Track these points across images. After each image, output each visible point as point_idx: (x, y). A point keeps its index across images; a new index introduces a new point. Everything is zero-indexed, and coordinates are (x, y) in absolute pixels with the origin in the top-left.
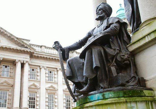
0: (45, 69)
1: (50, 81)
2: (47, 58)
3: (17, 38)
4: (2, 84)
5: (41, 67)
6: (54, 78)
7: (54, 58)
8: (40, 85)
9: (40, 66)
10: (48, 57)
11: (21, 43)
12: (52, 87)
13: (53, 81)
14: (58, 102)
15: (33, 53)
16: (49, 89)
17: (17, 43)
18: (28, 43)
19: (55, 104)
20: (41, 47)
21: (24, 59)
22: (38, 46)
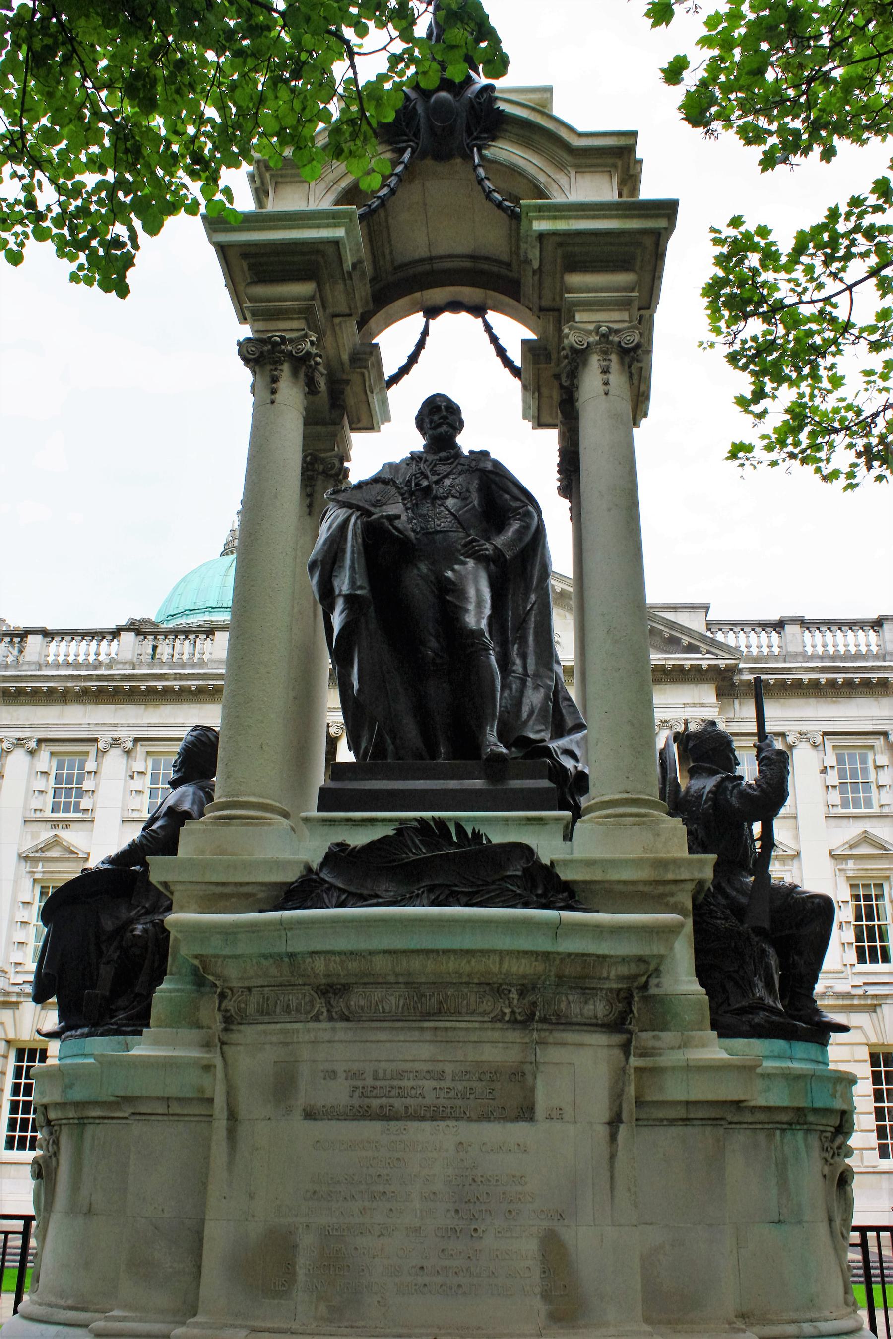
0: (815, 746)
1: (852, 811)
4: (42, 850)
6: (873, 787)
7: (857, 677)
8: (797, 837)
10: (823, 678)
11: (662, 628)
12: (866, 838)
13: (875, 810)
15: (733, 670)
16: (850, 857)
18: (695, 623)
20: (779, 625)
21: (690, 713)
22: (764, 626)
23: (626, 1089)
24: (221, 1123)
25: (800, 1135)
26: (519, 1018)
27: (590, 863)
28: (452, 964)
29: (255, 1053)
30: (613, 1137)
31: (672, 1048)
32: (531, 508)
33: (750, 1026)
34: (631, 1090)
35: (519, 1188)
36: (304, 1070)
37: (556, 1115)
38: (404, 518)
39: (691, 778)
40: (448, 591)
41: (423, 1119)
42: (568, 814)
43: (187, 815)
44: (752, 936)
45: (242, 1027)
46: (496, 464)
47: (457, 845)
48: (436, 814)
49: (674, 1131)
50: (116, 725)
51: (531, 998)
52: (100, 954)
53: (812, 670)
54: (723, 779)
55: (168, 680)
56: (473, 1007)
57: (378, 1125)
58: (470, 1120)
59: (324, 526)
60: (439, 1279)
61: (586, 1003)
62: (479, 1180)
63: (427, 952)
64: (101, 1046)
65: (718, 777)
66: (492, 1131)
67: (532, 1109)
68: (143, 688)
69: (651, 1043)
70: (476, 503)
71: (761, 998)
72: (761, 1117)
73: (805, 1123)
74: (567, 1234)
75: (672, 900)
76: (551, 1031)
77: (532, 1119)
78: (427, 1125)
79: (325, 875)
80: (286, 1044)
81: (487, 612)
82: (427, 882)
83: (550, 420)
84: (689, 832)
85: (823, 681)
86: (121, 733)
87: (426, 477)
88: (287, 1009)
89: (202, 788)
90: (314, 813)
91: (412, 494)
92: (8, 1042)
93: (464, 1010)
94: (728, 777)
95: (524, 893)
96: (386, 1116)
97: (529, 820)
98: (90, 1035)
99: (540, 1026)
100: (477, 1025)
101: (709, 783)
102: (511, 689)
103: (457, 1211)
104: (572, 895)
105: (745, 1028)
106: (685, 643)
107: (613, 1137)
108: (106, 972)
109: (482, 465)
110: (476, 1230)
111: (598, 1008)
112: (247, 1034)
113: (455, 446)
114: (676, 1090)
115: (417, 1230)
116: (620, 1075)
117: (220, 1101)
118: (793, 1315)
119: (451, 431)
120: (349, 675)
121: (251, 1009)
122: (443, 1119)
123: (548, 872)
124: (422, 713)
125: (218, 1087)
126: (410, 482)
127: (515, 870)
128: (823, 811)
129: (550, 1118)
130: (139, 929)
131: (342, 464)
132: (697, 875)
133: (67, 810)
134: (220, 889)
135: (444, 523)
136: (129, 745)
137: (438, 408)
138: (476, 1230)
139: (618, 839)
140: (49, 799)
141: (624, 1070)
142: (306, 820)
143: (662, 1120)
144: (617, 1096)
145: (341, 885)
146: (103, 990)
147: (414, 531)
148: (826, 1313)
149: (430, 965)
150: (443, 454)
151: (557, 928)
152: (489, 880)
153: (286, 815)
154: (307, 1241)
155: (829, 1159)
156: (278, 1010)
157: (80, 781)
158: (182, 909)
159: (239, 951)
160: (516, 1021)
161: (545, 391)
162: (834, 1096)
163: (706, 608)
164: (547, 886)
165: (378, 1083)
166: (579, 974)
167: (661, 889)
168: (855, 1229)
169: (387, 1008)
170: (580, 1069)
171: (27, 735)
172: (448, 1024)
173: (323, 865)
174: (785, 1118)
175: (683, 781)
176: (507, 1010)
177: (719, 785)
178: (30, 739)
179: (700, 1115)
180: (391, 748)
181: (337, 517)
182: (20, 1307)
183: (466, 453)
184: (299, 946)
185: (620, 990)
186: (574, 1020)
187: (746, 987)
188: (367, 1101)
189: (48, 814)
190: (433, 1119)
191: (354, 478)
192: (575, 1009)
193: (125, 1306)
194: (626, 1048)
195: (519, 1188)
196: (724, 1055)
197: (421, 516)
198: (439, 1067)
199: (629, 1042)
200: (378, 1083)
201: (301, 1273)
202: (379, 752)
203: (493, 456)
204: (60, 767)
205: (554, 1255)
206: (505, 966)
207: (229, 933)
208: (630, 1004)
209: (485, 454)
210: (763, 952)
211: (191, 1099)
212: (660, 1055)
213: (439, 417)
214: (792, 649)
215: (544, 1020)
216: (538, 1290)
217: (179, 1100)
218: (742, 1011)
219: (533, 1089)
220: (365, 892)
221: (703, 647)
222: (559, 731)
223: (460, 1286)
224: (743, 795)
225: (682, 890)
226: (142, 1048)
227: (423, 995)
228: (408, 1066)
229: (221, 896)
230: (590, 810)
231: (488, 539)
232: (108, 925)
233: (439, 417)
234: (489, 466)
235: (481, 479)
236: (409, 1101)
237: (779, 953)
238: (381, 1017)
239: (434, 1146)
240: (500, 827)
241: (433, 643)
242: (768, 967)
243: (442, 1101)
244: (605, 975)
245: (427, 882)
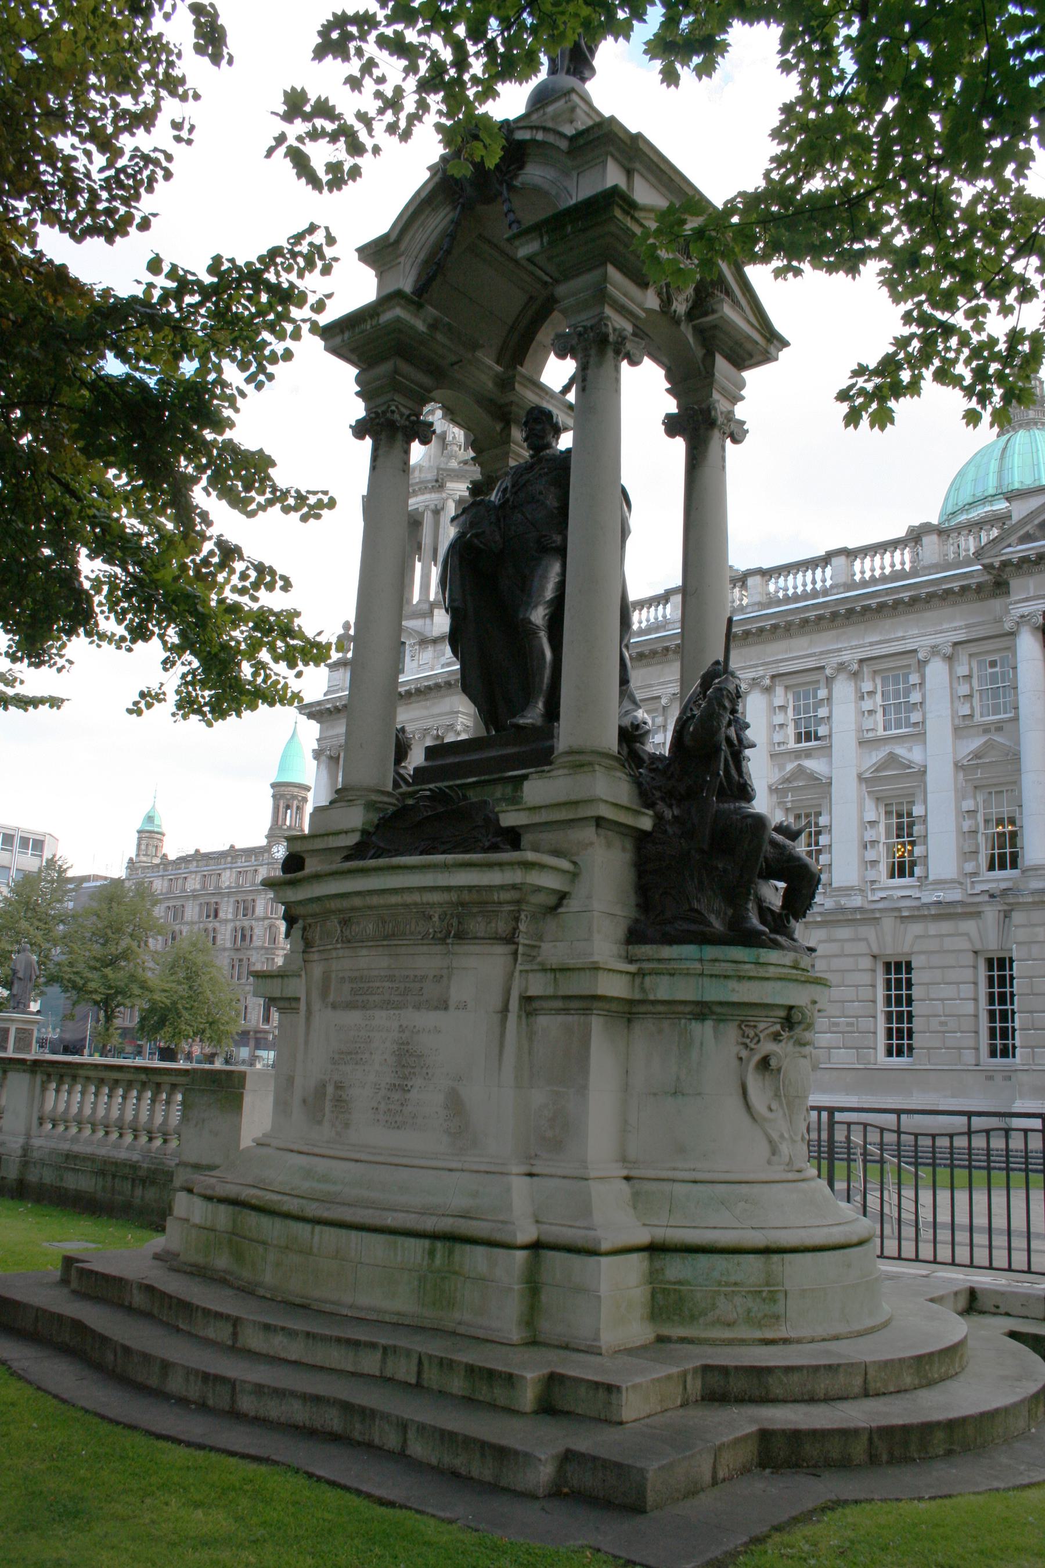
37: (463, 1006)
50: (840, 650)
55: (880, 596)
68: (858, 609)
77: (446, 1008)
86: (846, 657)
92: (874, 957)
129: (457, 1008)
136: (855, 667)
168: (813, 1108)
171: (761, 673)
178: (763, 677)
205: (455, 1105)
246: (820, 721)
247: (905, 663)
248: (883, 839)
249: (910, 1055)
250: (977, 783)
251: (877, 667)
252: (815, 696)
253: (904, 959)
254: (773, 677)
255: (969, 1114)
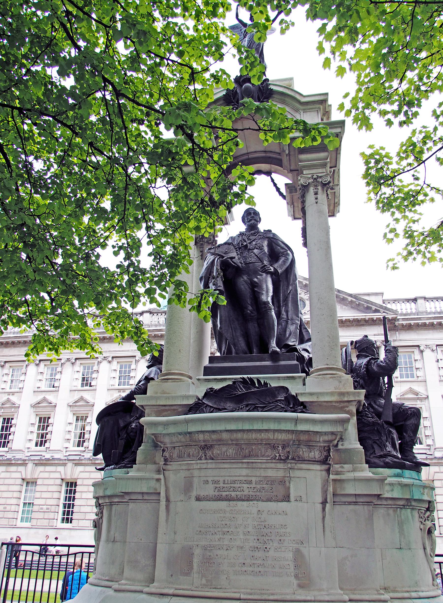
0: (433, 351)
2: (432, 325)
3: (351, 295)
5: (422, 348)
8: (427, 390)
9: (418, 346)
14: (431, 427)
15: (395, 319)
17: (355, 305)
18: (378, 300)
19: (426, 432)
20: (415, 300)
22: (408, 300)
23: (329, 488)
24: (163, 502)
25: (409, 510)
26: (282, 458)
27: (311, 394)
28: (254, 436)
29: (176, 474)
30: (324, 509)
31: (349, 472)
32: (289, 252)
33: (384, 463)
34: (331, 489)
35: (284, 530)
36: (196, 480)
37: (299, 499)
38: (237, 258)
39: (358, 359)
40: (256, 287)
41: (243, 500)
42: (305, 374)
43: (153, 379)
44: (385, 425)
45: (171, 463)
46: (274, 235)
47: (257, 388)
48: (249, 376)
49: (351, 507)
51: (288, 449)
52: (119, 436)
53: (430, 318)
54: (370, 359)
56: (263, 454)
57: (225, 503)
58: (263, 501)
59: (206, 262)
60: (251, 569)
61: (311, 452)
62: (267, 526)
63: (243, 431)
64: (118, 472)
65: (368, 358)
66: (272, 505)
67: (289, 496)
69: (340, 470)
70: (266, 251)
71: (389, 452)
72: (390, 502)
73: (411, 506)
74: (305, 551)
75: (347, 409)
76: (296, 463)
78: (245, 503)
79: (205, 401)
80: (189, 470)
81: (271, 294)
82: (245, 403)
83: (299, 217)
84: (355, 382)
85: (435, 323)
87: (246, 241)
88: (189, 456)
89: (159, 369)
90: (202, 377)
91: (240, 248)
93: (260, 455)
94: (372, 359)
95: (285, 407)
96: (229, 499)
97: (288, 377)
98: (114, 468)
99: (291, 461)
100: (265, 461)
101: (364, 361)
102: (282, 325)
103: (258, 539)
104: (305, 407)
105: (382, 464)
106: (374, 309)
107: (324, 509)
108: (122, 443)
109: (268, 236)
110: (266, 548)
111: (316, 454)
112: (173, 466)
113: (257, 228)
114: (350, 489)
115: (242, 548)
116: (326, 483)
117: (163, 494)
118: (407, 589)
119: (256, 222)
120: (217, 321)
121: (175, 456)
122: (252, 500)
123: (295, 398)
124: (247, 336)
125: (162, 488)
126: (241, 244)
127: (281, 397)
128: (438, 378)
129: (296, 500)
130: (134, 425)
131: (214, 238)
132: (357, 398)
133: (124, 385)
134: (164, 408)
135: (253, 259)
137: (250, 214)
138: (266, 548)
139: (327, 385)
140: (117, 380)
141: (328, 481)
142: (199, 380)
143: (345, 502)
144: (325, 492)
145: (211, 405)
146: (120, 450)
147: (241, 263)
148: (423, 589)
149: (245, 436)
150: (253, 232)
151: (296, 421)
152: (271, 402)
153: (190, 378)
154: (197, 552)
155: (423, 522)
156: (185, 455)
157: (129, 373)
158: (149, 416)
159: (169, 432)
160: (281, 459)
161: (296, 204)
162: (423, 494)
163: (382, 294)
164: (294, 403)
165: (225, 486)
166: (306, 439)
167: (342, 405)
169: (228, 455)
170: (309, 480)
172: (253, 461)
173: (204, 397)
174: (401, 503)
175: (354, 359)
176: (277, 455)
177: (369, 362)
179: (361, 500)
180: (233, 350)
181: (210, 259)
182: (89, 580)
183: (262, 231)
184: (192, 428)
185: (325, 447)
186: (306, 459)
187: (382, 446)
188: (221, 493)
189: (117, 387)
190: (248, 500)
191: (219, 243)
192: (306, 455)
193: (127, 579)
194: (328, 471)
195: (284, 530)
196: (371, 474)
197: (244, 257)
198: (250, 479)
199: (329, 468)
200: (225, 486)
201: (195, 565)
202: (229, 351)
203: (273, 232)
204: (121, 367)
205: (299, 558)
206: (276, 436)
207: (166, 424)
208: (329, 452)
209: (270, 231)
210: (390, 431)
211: (152, 493)
212: (344, 474)
213: (251, 217)
214: (421, 310)
215: (293, 459)
216: (292, 574)
217: (147, 493)
218: (381, 456)
219: (289, 488)
220: (220, 407)
221: (382, 310)
222: (302, 341)
223: (260, 572)
224: (379, 366)
225: (351, 405)
226: (133, 472)
227: (243, 449)
228: (237, 478)
229: (162, 410)
230: (313, 373)
231: (271, 265)
232: (122, 424)
233: (251, 217)
234: (271, 236)
235: (268, 241)
236: (238, 493)
237: (397, 432)
238: (225, 458)
239: (248, 512)
240: (274, 381)
241: (250, 308)
242: (393, 439)
243: (251, 493)
244: (318, 440)
245: (245, 403)
246: (55, 380)
247: (22, 364)
248: (36, 431)
249: (71, 522)
250: (74, 412)
251: (11, 365)
252: (92, 369)
253: (74, 481)
254: (113, 357)
255: (69, 546)
